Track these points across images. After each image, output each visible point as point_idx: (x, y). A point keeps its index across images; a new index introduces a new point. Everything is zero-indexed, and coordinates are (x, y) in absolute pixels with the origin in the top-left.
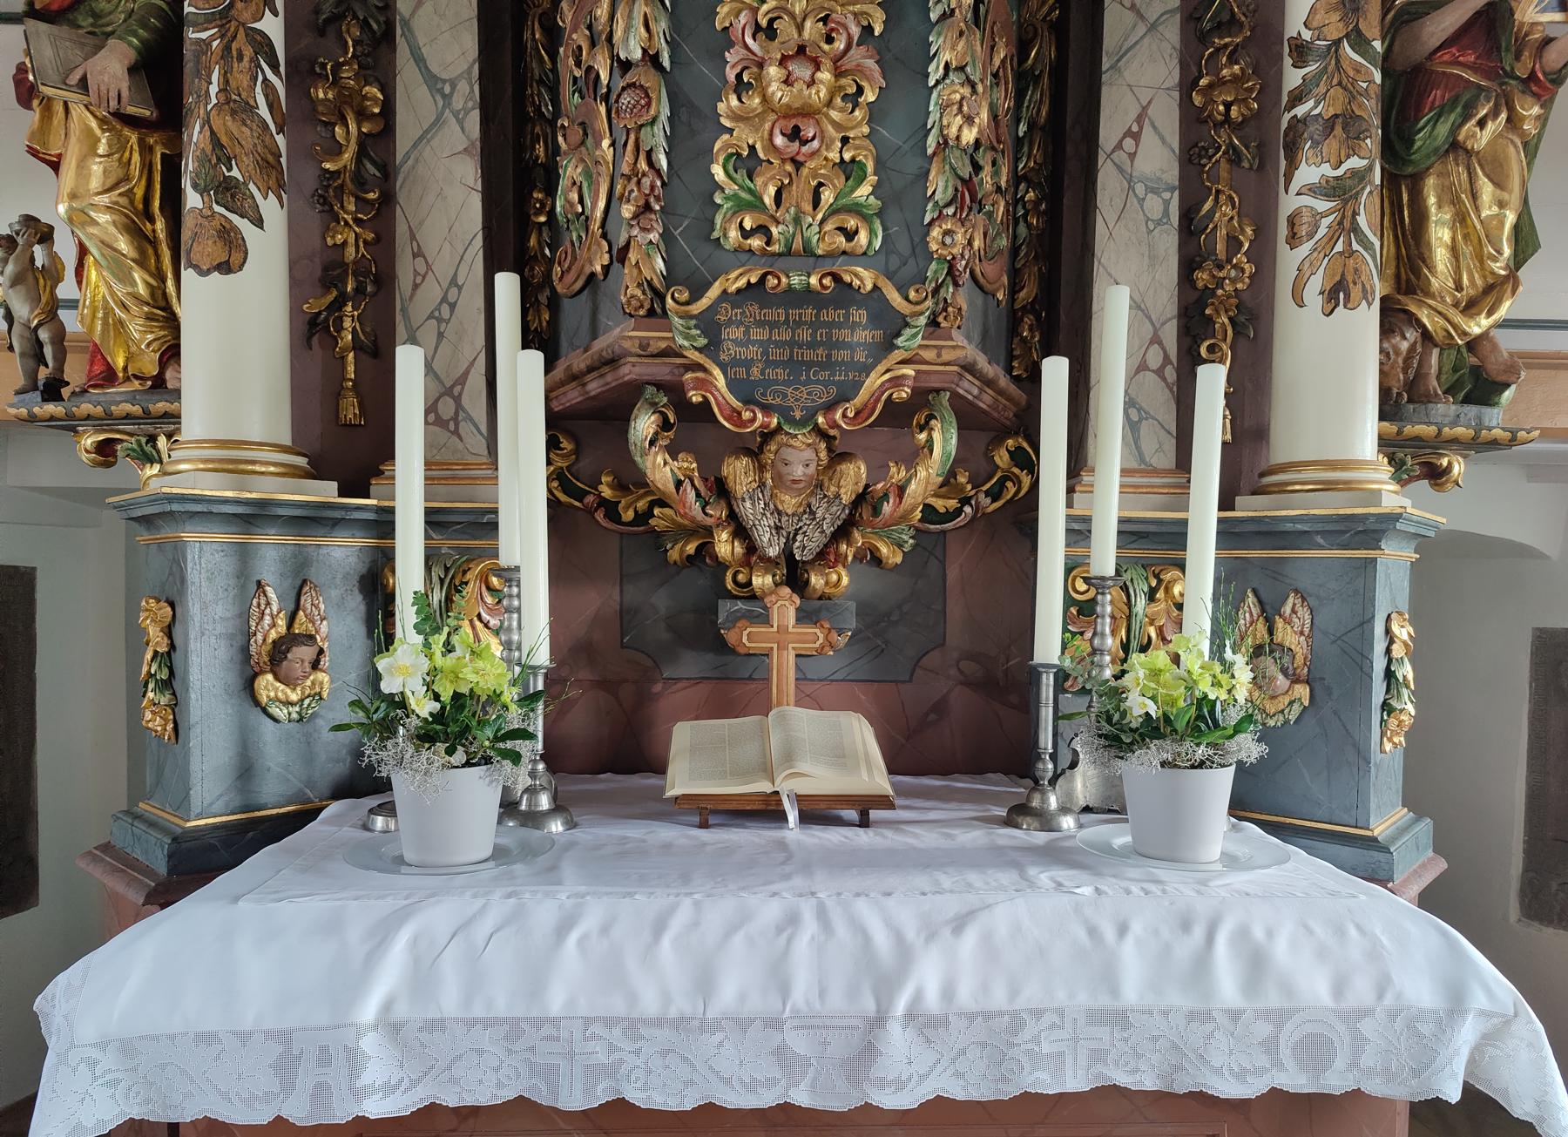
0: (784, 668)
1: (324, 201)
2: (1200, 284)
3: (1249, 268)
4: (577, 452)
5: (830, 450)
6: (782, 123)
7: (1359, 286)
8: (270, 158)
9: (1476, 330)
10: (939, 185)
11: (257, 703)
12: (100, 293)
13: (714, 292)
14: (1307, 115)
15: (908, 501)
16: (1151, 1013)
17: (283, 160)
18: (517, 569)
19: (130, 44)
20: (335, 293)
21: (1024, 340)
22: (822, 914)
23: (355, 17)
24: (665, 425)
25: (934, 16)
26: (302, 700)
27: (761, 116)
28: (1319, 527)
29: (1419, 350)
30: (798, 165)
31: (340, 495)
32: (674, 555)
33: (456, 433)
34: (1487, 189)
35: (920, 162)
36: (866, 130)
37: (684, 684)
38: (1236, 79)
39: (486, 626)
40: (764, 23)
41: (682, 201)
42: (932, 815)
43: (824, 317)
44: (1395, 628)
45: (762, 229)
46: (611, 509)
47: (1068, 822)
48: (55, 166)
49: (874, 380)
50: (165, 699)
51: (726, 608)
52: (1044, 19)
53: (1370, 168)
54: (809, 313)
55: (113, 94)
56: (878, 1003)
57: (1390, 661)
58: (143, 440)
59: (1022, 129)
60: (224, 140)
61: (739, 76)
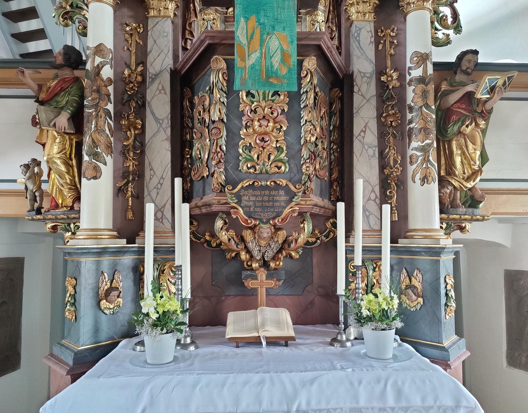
0: (262, 294)
1: (124, 153)
2: (386, 173)
3: (401, 169)
4: (198, 225)
5: (275, 228)
6: (259, 136)
7: (431, 177)
8: (109, 145)
9: (470, 186)
10: (305, 153)
11: (100, 309)
12: (55, 184)
13: (239, 187)
14: (413, 127)
15: (298, 245)
16: (368, 409)
17: (112, 145)
18: (181, 266)
19: (68, 113)
20: (126, 180)
21: (334, 189)
22: (272, 380)
23: (134, 100)
24: (225, 223)
25: (302, 106)
26: (114, 307)
27: (253, 135)
28: (422, 250)
29: (453, 192)
30: (264, 148)
31: (127, 244)
32: (228, 256)
33: (162, 222)
34: (470, 146)
35: (299, 146)
36: (283, 138)
37: (232, 297)
38: (394, 114)
39: (171, 282)
40: (253, 109)
41: (231, 158)
42: (308, 341)
43: (272, 193)
44: (447, 280)
45: (253, 167)
46: (209, 243)
47: (349, 344)
48: (44, 145)
49: (287, 211)
50: (73, 309)
51: (244, 273)
52: (337, 96)
53: (433, 143)
54: (267, 192)
55: (63, 128)
56: (288, 407)
57: (447, 290)
58: (66, 225)
59: (331, 128)
60: (96, 141)
61: (246, 124)
